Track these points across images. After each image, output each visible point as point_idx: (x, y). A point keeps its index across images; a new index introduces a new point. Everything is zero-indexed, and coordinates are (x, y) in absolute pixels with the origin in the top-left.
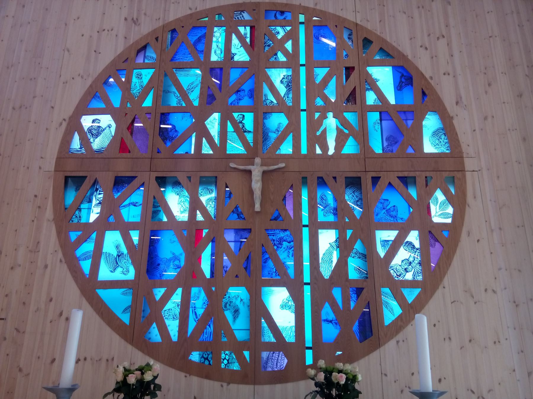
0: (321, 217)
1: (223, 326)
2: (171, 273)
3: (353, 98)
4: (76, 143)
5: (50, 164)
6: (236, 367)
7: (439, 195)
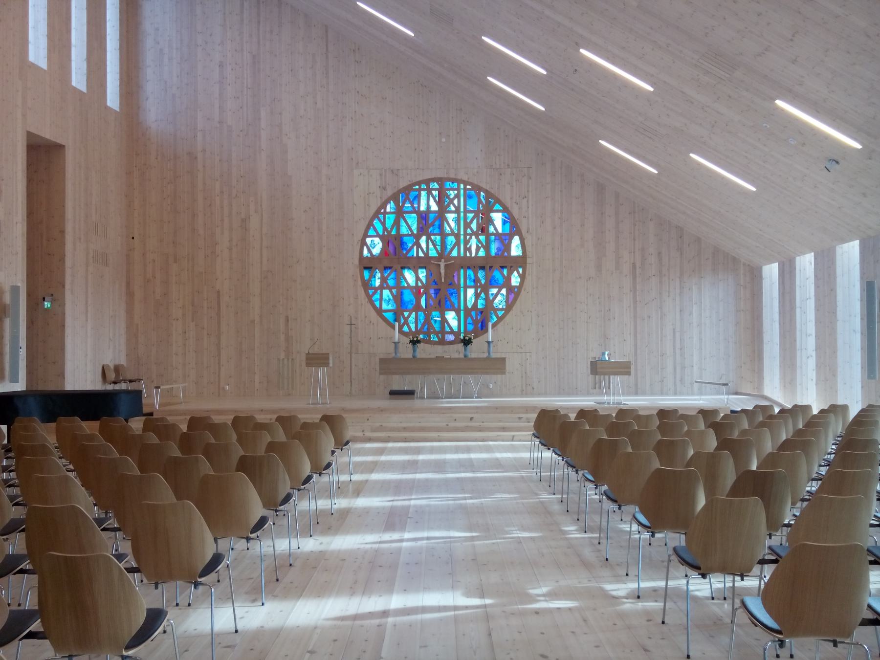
0: (469, 283)
1: (430, 326)
2: (410, 307)
3: (483, 230)
4: (365, 252)
5: (357, 262)
6: (436, 339)
7: (515, 273)
